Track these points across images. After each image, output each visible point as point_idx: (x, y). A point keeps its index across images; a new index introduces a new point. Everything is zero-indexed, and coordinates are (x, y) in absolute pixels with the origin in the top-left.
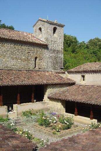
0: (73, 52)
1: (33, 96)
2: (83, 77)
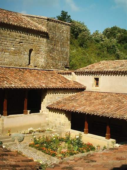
0: (81, 45)
1: (26, 105)
2: (97, 80)
